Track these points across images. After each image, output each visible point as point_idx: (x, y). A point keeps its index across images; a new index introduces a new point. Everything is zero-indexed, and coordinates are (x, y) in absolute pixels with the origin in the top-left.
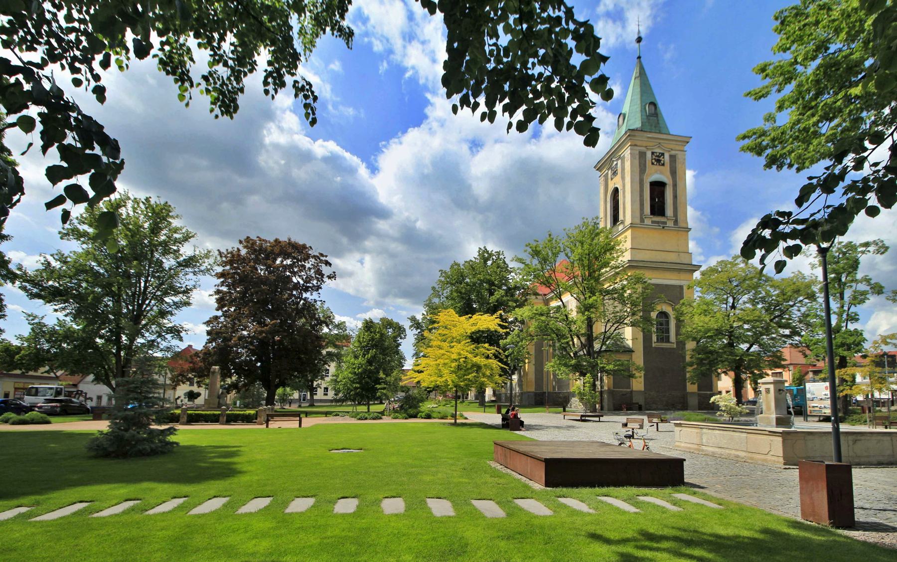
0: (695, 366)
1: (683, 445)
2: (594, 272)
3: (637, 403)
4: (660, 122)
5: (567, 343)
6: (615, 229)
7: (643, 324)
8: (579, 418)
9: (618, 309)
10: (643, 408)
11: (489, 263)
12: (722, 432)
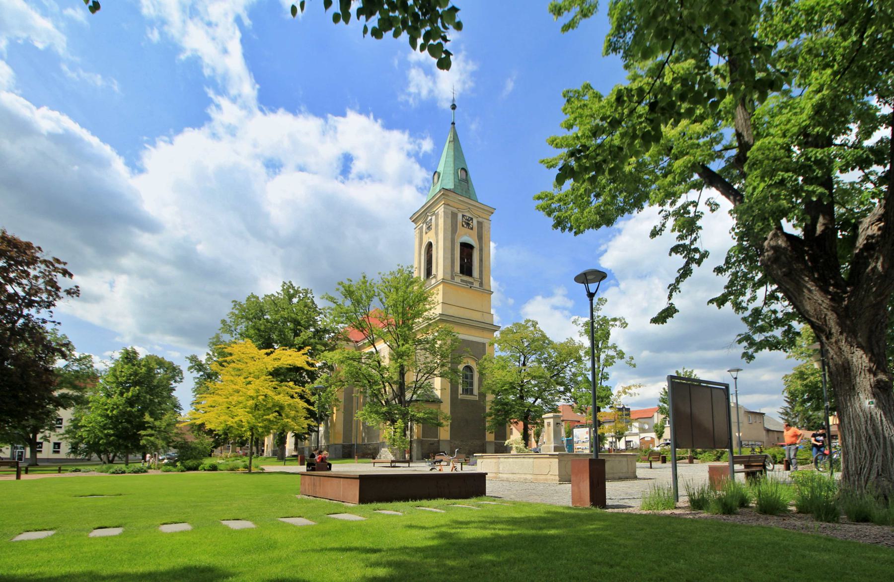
0: (493, 417)
2: (408, 320)
5: (379, 390)
6: (428, 282)
7: (450, 375)
8: (389, 465)
9: (429, 360)
11: (295, 300)
12: (514, 460)
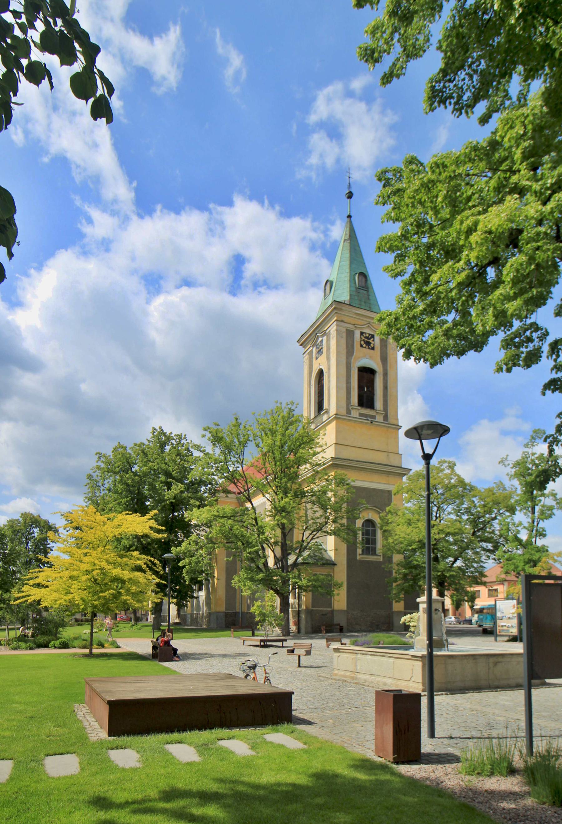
1: (340, 673)
3: (339, 625)
4: (371, 297)
6: (319, 419)
8: (258, 643)
10: (344, 630)
11: (168, 448)
12: (373, 657)
